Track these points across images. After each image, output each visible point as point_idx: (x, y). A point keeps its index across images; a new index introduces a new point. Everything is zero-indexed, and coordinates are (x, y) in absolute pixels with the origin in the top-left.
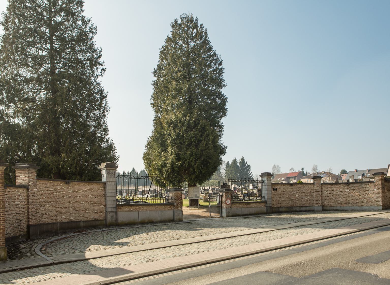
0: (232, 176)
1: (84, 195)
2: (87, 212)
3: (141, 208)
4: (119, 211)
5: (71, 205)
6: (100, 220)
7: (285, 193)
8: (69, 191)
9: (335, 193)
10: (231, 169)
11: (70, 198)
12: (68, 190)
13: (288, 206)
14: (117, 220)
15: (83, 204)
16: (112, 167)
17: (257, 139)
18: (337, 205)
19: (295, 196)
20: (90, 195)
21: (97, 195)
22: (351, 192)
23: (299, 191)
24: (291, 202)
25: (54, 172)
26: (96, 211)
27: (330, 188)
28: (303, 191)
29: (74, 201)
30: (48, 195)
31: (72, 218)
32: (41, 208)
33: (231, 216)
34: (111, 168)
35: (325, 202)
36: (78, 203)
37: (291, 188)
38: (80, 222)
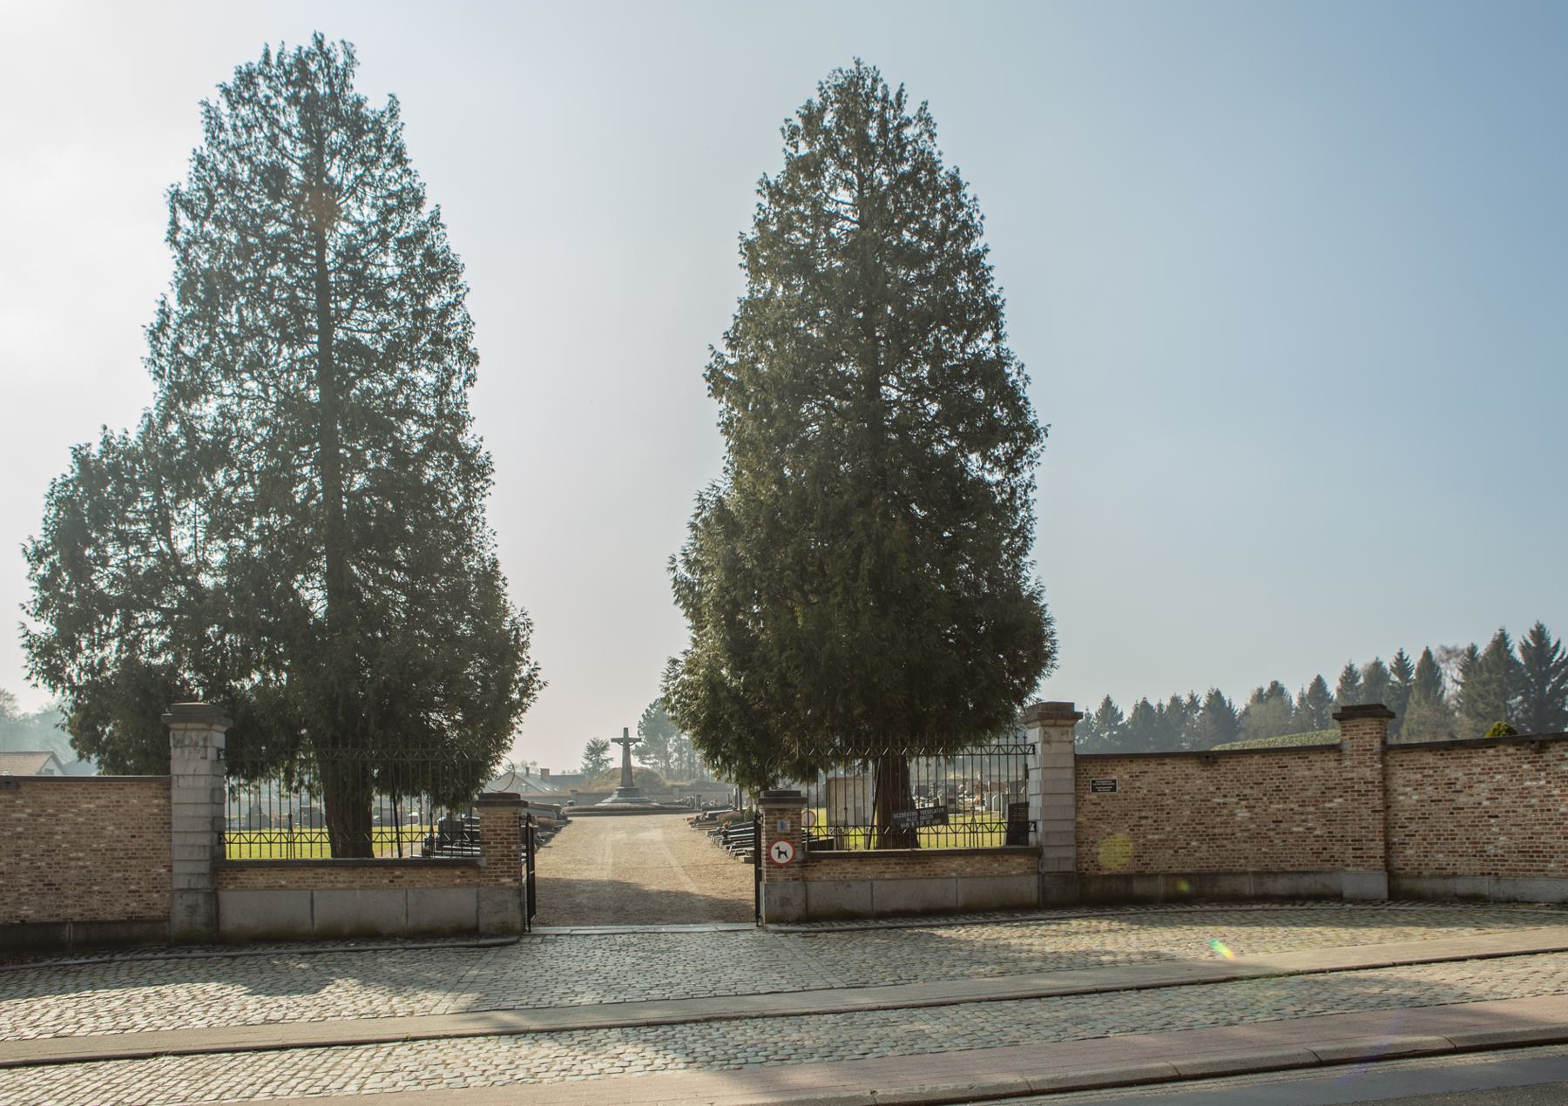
6: (148, 922)
9: (1462, 799)
10: (1486, 675)
13: (1187, 870)
14: (215, 918)
15: (79, 859)
16: (190, 721)
17: (1184, 558)
18: (1476, 865)
22: (1556, 792)
23: (1256, 792)
24: (1204, 847)
26: (133, 887)
27: (1435, 769)
28: (1278, 789)
31: (28, 912)
33: (798, 922)
34: (190, 726)
35: (1409, 852)
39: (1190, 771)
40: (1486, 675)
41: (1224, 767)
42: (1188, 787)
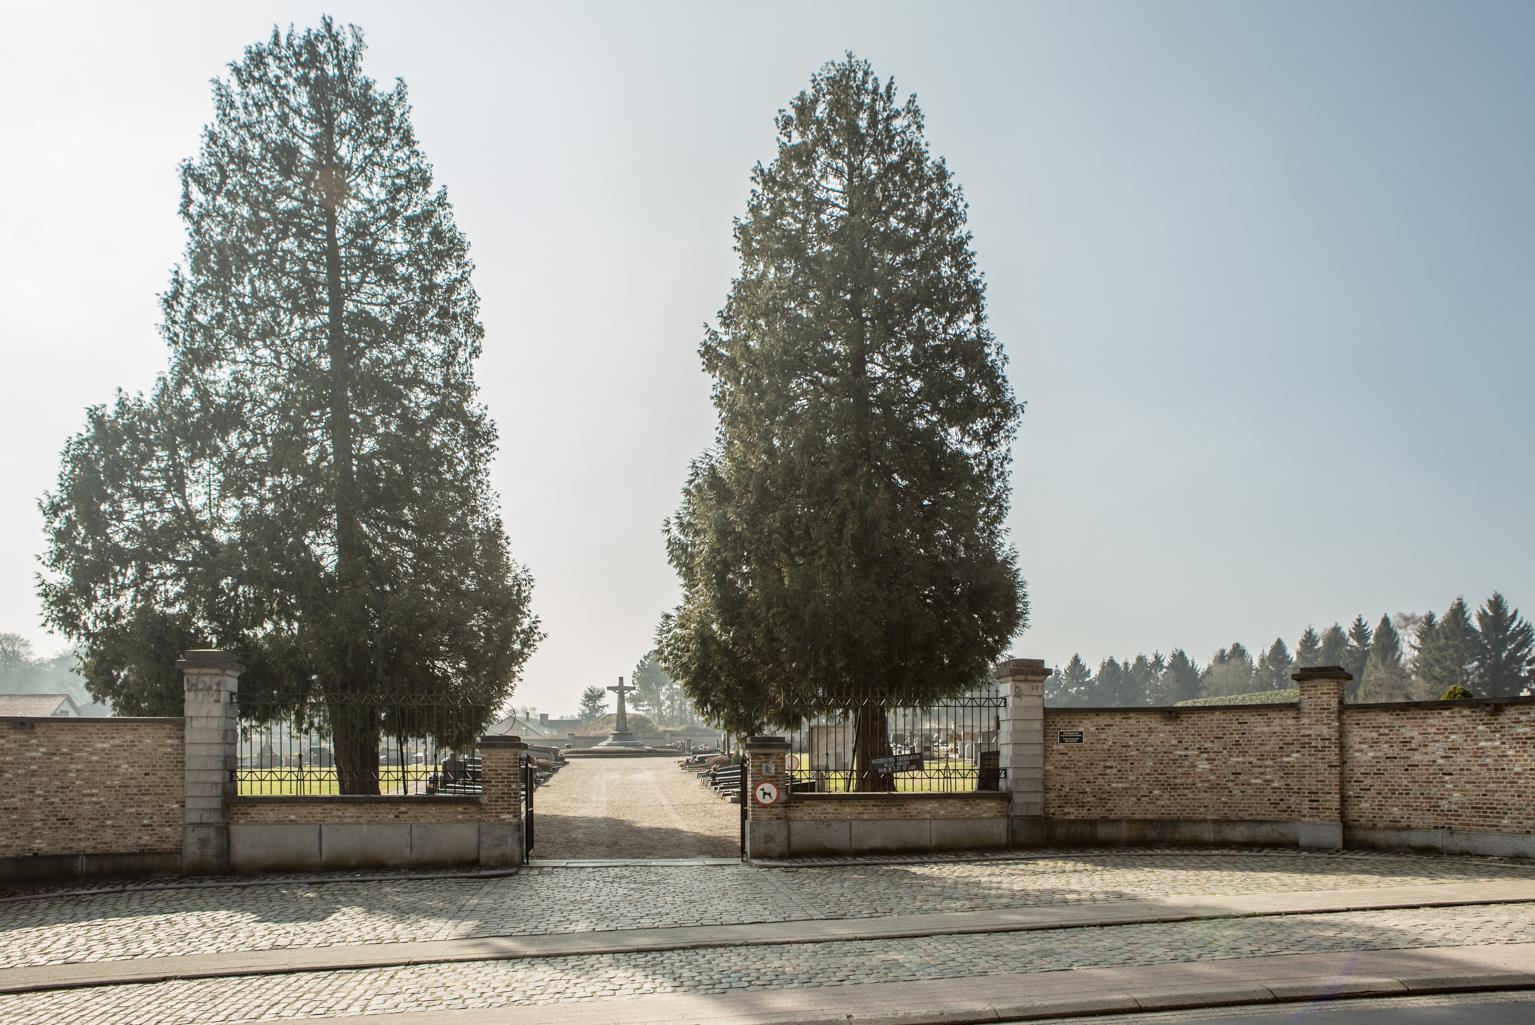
0: (1443, 668)
2: (109, 822)
3: (334, 813)
4: (241, 821)
7: (1135, 753)
9: (1417, 757)
11: (33, 776)
12: (28, 750)
13: (1149, 817)
14: (226, 850)
15: (92, 795)
18: (1430, 819)
20: (125, 766)
21: (154, 766)
22: (1511, 752)
23: (1216, 746)
24: (1166, 796)
26: (146, 822)
27: (1391, 728)
28: (1237, 744)
29: (52, 788)
31: (40, 845)
33: (781, 857)
35: (1364, 805)
37: (1168, 728)
38: (76, 856)
39: (1153, 725)
40: (1443, 641)
41: (1186, 721)
42: (1151, 740)
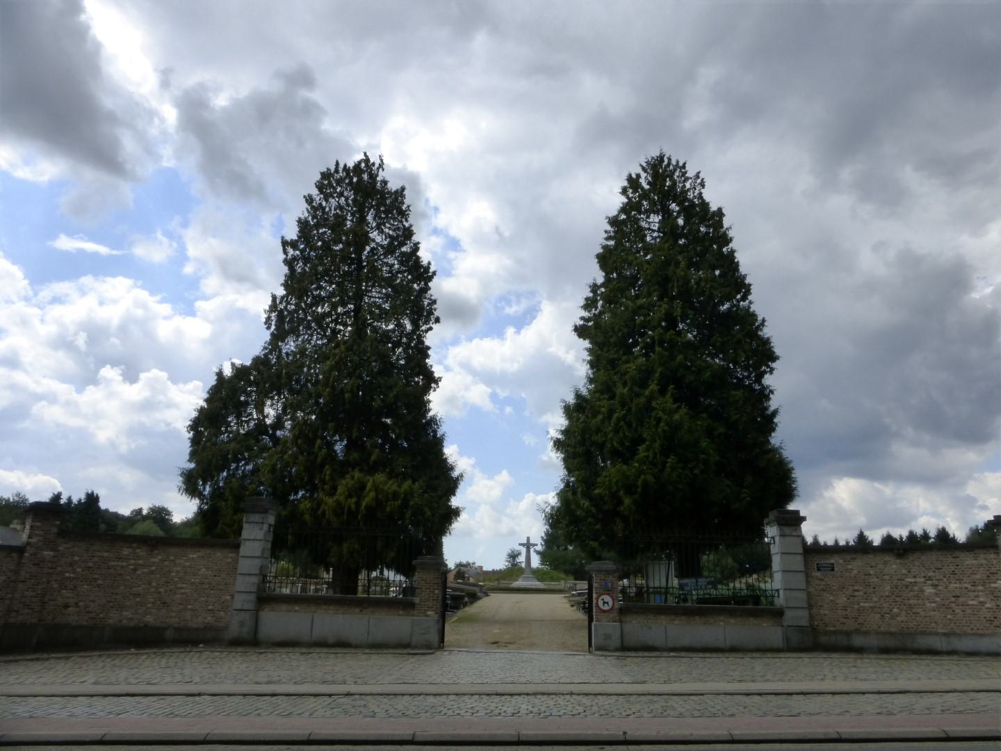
1: (189, 569)
2: (189, 607)
5: (153, 590)
7: (875, 580)
8: (153, 560)
13: (893, 630)
15: (182, 588)
19: (922, 591)
20: (203, 570)
24: (903, 613)
25: (618, 520)
26: (210, 607)
28: (954, 573)
30: (90, 564)
31: (149, 619)
32: (64, 591)
36: (170, 587)
